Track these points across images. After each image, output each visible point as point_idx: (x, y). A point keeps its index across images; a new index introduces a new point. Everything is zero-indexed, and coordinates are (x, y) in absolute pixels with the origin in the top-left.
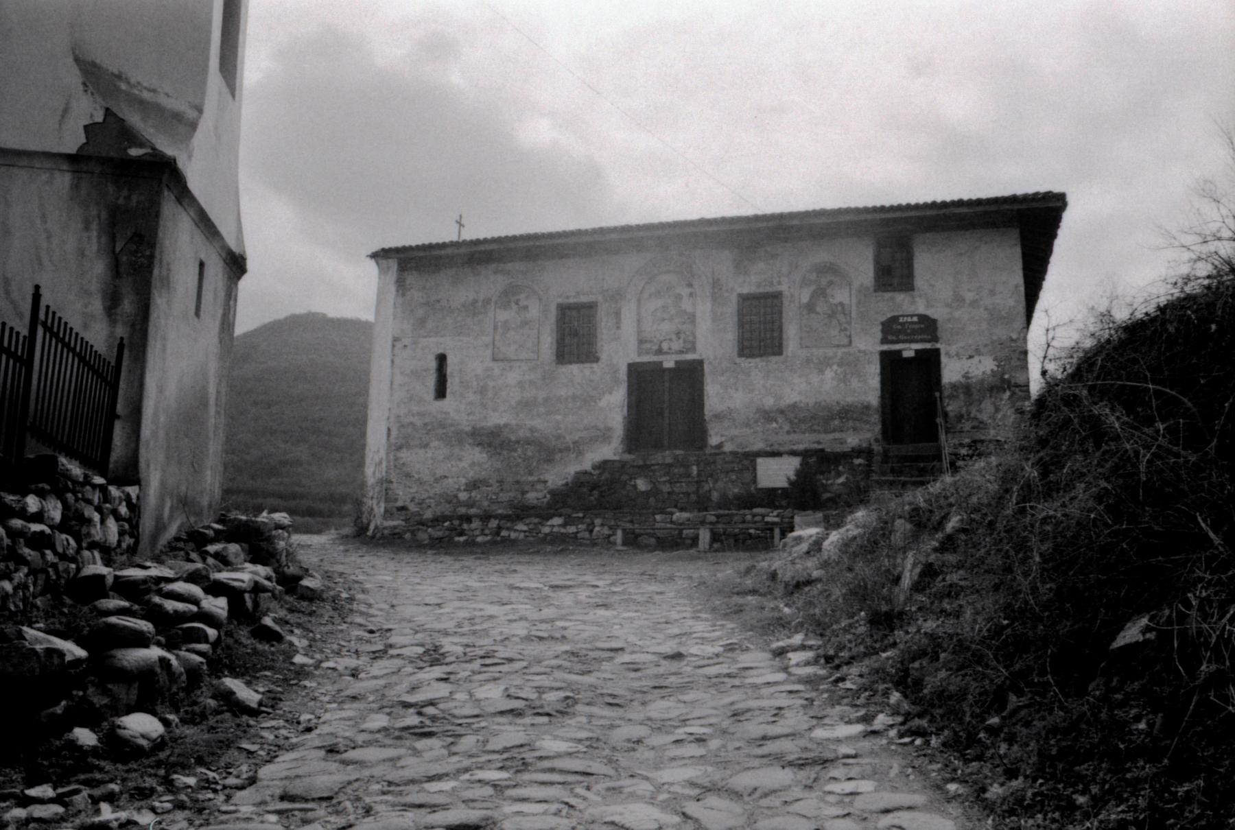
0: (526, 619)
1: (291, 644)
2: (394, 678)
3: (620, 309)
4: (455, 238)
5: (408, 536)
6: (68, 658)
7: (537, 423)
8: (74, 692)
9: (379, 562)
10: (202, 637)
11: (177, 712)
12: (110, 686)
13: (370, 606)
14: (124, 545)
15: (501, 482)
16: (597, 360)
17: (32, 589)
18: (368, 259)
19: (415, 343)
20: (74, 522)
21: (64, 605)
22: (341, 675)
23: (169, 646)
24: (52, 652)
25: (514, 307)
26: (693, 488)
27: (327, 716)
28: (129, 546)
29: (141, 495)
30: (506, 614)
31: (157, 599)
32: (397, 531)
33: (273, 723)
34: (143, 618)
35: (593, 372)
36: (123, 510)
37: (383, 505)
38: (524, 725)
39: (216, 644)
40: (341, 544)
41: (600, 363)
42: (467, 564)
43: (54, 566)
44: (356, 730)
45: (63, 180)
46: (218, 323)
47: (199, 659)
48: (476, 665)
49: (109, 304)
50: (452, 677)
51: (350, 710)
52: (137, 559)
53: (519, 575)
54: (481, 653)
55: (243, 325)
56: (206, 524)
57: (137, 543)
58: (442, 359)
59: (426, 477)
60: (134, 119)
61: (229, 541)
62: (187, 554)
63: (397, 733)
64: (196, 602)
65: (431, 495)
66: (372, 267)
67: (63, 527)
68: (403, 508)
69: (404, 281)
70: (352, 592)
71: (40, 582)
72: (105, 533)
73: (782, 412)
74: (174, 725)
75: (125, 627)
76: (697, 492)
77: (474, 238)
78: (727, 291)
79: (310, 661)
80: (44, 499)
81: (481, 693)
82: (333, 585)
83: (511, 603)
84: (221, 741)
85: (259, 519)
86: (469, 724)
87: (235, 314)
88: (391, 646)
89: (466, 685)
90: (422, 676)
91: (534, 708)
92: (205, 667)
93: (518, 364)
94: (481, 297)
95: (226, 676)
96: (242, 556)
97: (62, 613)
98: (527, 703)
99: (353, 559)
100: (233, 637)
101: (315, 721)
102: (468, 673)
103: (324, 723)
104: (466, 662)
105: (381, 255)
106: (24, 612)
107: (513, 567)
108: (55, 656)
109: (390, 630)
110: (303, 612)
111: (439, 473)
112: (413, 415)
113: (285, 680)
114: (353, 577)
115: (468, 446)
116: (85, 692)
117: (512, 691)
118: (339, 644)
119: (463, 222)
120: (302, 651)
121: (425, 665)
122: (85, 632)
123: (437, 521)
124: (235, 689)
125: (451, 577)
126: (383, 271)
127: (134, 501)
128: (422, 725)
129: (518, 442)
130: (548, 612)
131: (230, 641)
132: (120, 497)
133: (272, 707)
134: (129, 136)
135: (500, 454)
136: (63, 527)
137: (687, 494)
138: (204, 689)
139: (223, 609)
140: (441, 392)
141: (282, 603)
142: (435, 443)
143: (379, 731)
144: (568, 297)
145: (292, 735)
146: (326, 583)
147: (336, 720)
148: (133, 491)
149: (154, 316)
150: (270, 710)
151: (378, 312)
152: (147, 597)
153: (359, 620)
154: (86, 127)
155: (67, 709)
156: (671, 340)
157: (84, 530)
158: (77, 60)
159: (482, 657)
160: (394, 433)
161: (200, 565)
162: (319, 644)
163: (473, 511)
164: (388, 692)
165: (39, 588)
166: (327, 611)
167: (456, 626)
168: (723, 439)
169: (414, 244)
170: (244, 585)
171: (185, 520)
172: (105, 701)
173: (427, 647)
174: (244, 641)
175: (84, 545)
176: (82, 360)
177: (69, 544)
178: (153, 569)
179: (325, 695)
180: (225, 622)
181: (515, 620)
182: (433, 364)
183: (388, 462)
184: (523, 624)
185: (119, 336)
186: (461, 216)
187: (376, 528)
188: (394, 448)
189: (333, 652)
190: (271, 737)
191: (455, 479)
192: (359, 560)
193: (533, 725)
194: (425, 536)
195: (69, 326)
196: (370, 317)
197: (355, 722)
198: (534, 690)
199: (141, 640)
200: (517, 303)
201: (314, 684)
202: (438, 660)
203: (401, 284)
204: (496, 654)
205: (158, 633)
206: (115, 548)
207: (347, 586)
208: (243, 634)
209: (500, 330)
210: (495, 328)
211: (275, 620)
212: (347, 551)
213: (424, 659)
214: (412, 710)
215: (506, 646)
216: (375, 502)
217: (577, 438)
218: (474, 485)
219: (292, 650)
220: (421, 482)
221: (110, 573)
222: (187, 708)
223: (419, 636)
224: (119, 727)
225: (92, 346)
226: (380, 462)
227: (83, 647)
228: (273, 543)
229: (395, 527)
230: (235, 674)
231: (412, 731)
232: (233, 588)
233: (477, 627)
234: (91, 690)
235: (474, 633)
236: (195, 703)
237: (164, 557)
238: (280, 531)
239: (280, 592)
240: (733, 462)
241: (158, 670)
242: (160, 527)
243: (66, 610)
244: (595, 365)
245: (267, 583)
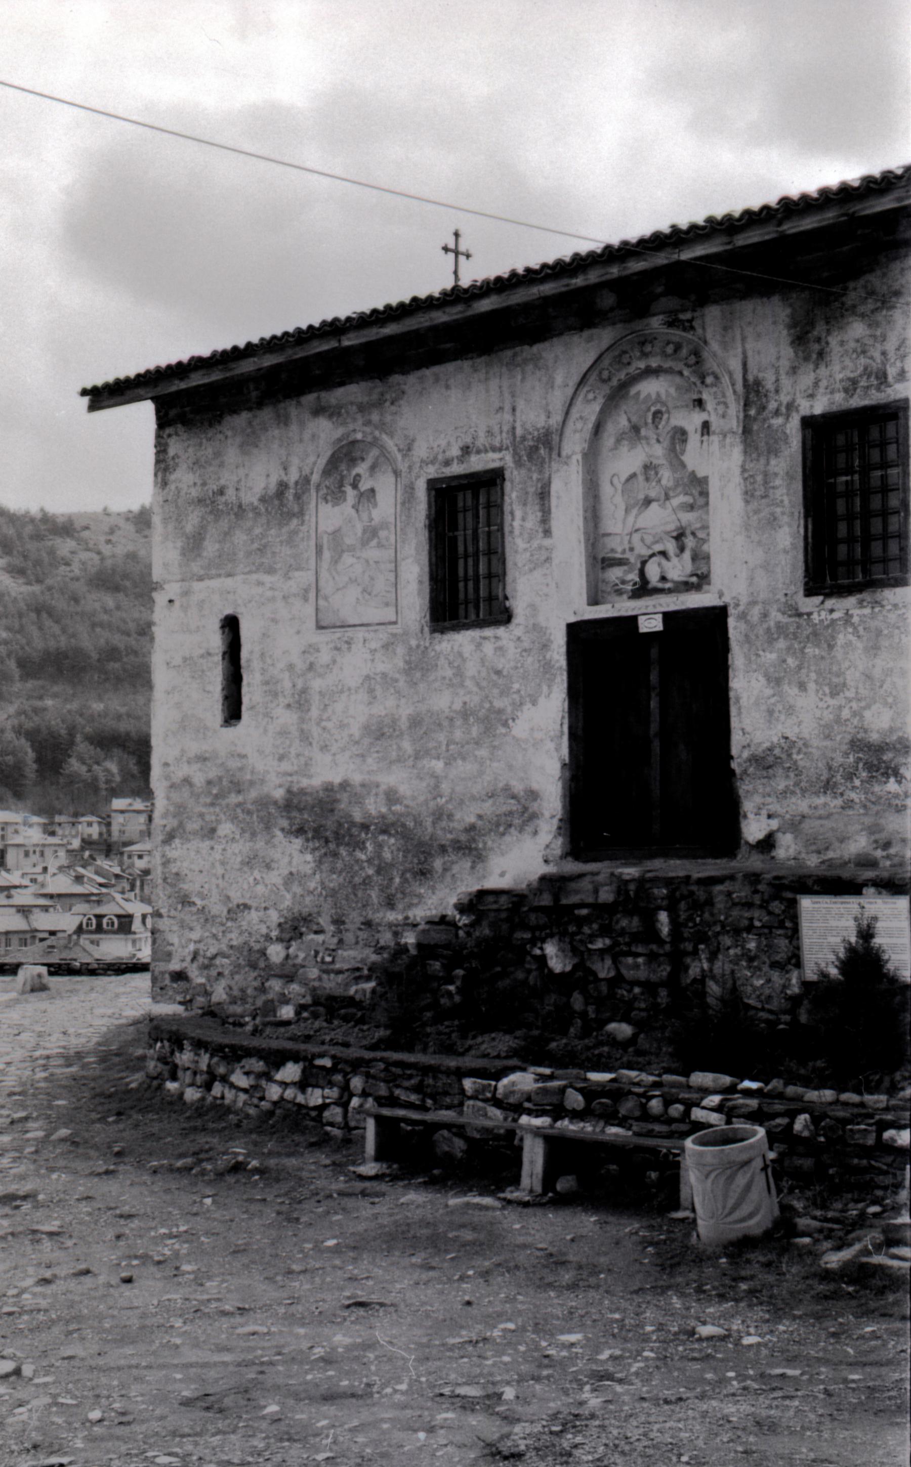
16: (504, 617)
19: (186, 593)
26: (664, 970)
41: (512, 626)
58: (231, 625)
59: (218, 909)
65: (224, 948)
68: (180, 976)
76: (673, 982)
78: (777, 413)
94: (293, 476)
111: (237, 897)
129: (365, 827)
135: (335, 855)
137: (650, 987)
144: (447, 463)
156: (663, 554)
168: (774, 824)
182: (216, 641)
200: (355, 486)
209: (327, 555)
217: (472, 819)
240: (749, 905)
244: (501, 631)
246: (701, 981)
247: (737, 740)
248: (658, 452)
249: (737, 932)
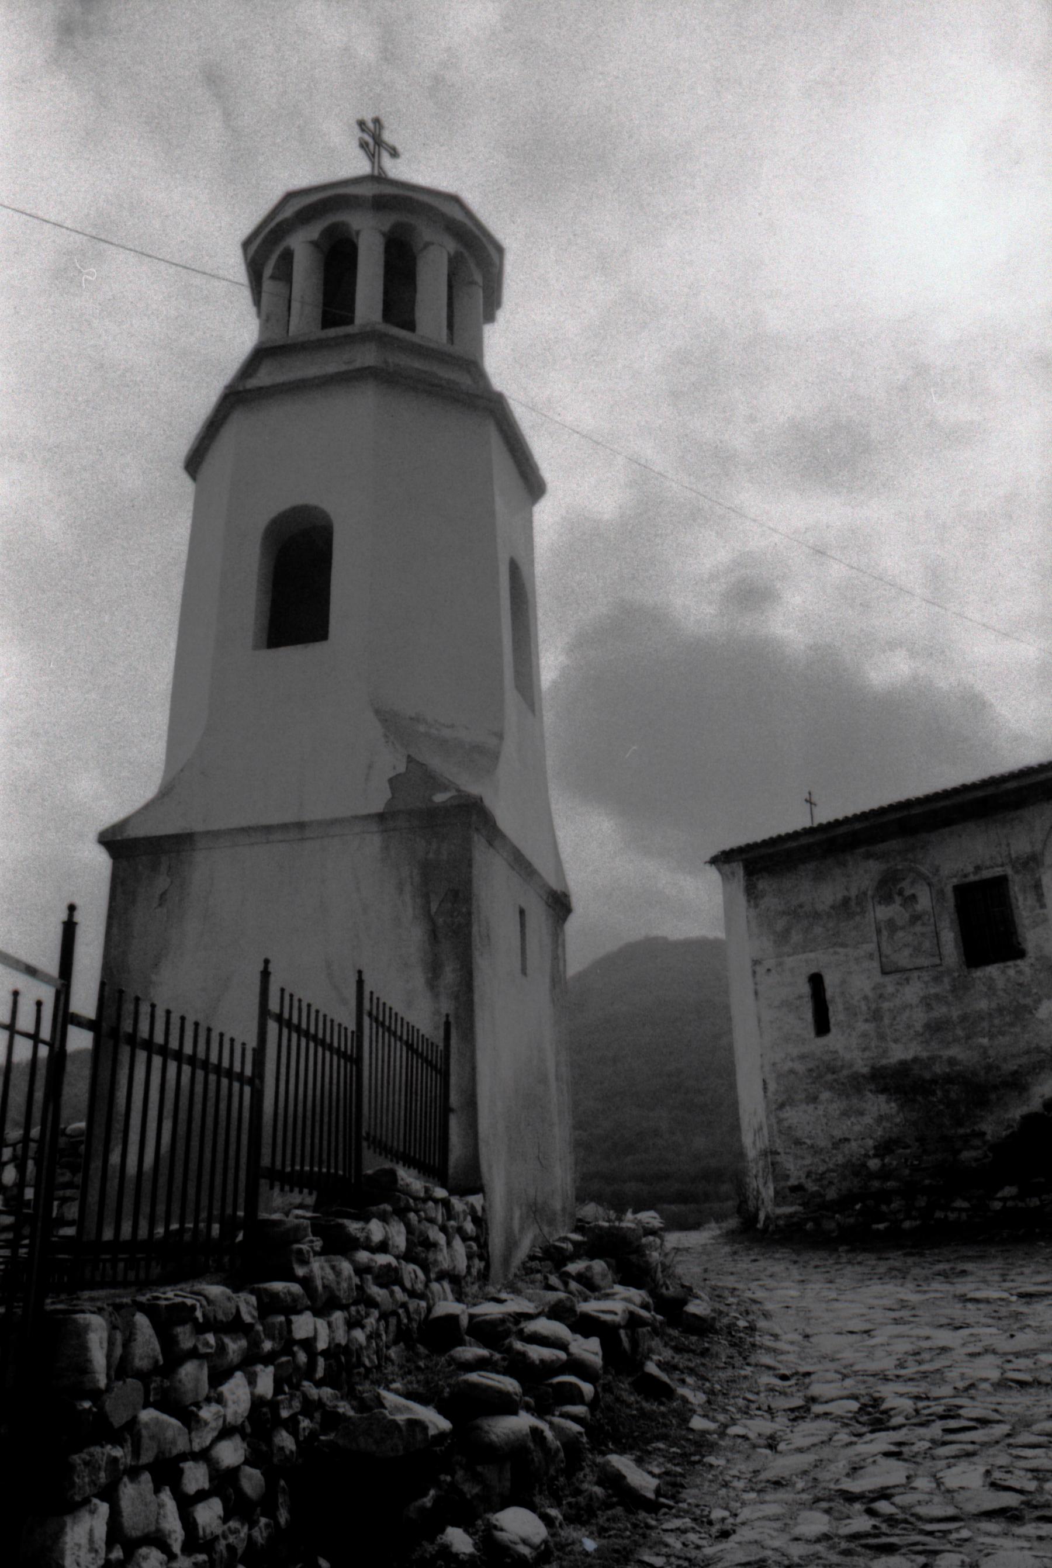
0: (994, 1352)
1: (685, 1400)
2: (826, 1452)
3: (1040, 880)
4: (808, 824)
5: (809, 1226)
6: (432, 1432)
7: (954, 1052)
8: (442, 1477)
9: (778, 1268)
10: (574, 1396)
11: (559, 1505)
12: (479, 1469)
13: (776, 1337)
14: (474, 1271)
15: (921, 1140)
16: (1021, 954)
17: (384, 1337)
18: (708, 867)
20: (420, 1249)
21: (418, 1355)
22: (754, 1446)
23: (541, 1410)
24: (415, 1424)
25: (898, 900)
27: (745, 1514)
28: (479, 1271)
29: (487, 1205)
30: (964, 1345)
31: (519, 1345)
32: (795, 1220)
33: (677, 1523)
34: (505, 1372)
35: (1020, 972)
36: (469, 1227)
37: (771, 1186)
38: (1028, 1538)
39: (593, 1404)
40: (726, 1244)
42: (897, 1264)
43: (404, 1305)
44: (787, 1537)
45: (374, 842)
46: (547, 980)
47: (576, 1428)
48: (936, 1429)
49: (430, 975)
50: (905, 1449)
51: (774, 1504)
52: (491, 1290)
53: (970, 1278)
54: (940, 1409)
55: (574, 965)
56: (562, 1235)
57: (488, 1267)
58: (816, 981)
59: (823, 1143)
60: (436, 763)
61: (592, 1258)
62: (546, 1278)
63: (844, 1545)
64: (563, 1346)
65: (831, 1166)
66: (713, 874)
67: (408, 1256)
69: (755, 887)
70: (751, 1317)
71: (392, 1328)
72: (453, 1259)
74: (557, 1524)
75: (489, 1388)
77: (831, 819)
79: (712, 1426)
80: (387, 1223)
81: (953, 1478)
82: (724, 1309)
83: (968, 1326)
84: (616, 1551)
85: (624, 1225)
86: (946, 1533)
87: (565, 966)
88: (813, 1400)
89: (928, 1463)
90: (861, 1448)
91: (1036, 1507)
92: (584, 1439)
93: (916, 974)
94: (853, 892)
95: (612, 1452)
96: (610, 1277)
97: (418, 1368)
98: (1023, 1498)
99: (745, 1266)
100: (612, 1393)
101: (731, 1520)
102: (928, 1445)
103: (743, 1524)
104: (921, 1425)
105: (722, 859)
106: (379, 1367)
107: (960, 1266)
108: (417, 1430)
109: (808, 1374)
110: (693, 1352)
111: (838, 1134)
112: (792, 1060)
113: (685, 1455)
114: (749, 1294)
115: (870, 1095)
116: (453, 1477)
117: (997, 1475)
118: (745, 1399)
119: (814, 799)
120: (699, 1410)
121: (864, 1429)
122: (446, 1395)
123: (844, 1202)
124: (625, 1471)
125: (876, 1288)
126: (726, 878)
127: (480, 1214)
128: (876, 1532)
129: (934, 1081)
130: (1025, 1340)
131: (609, 1398)
132: (464, 1211)
133: (673, 1497)
134: (432, 781)
136: (408, 1256)
138: (587, 1470)
139: (596, 1354)
140: (822, 1026)
141: (666, 1339)
142: (825, 1095)
143: (817, 1540)
144: (966, 876)
145: (704, 1543)
146: (717, 1306)
147: (759, 1519)
148: (476, 1200)
149: (477, 982)
150: (671, 1503)
151: (728, 929)
152: (507, 1341)
153: (767, 1360)
154: (390, 781)
155: (436, 1500)
157: (431, 1256)
158: (377, 712)
159: (942, 1418)
160: (772, 1086)
161: (562, 1295)
162: (720, 1398)
163: (891, 1184)
164: (824, 1475)
165: (391, 1336)
166: (722, 1348)
167: (896, 1366)
169: (759, 840)
170: (617, 1319)
171: (538, 1231)
172: (476, 1490)
173: (863, 1400)
174: (625, 1395)
175: (433, 1276)
176: (410, 1047)
177: (416, 1277)
178: (509, 1303)
179: (739, 1478)
180: (601, 1372)
181: (979, 1354)
182: (806, 989)
183: (770, 1126)
184: (990, 1359)
185: (444, 1012)
186: (810, 793)
187: (767, 1218)
188: (774, 1107)
189: (740, 1410)
190: (678, 1545)
191: (860, 1142)
192: (753, 1267)
193: (1040, 1538)
194: (832, 1225)
195: (393, 1012)
196: (720, 934)
197: (785, 1522)
198: (1029, 1475)
199: (507, 1405)
201: (722, 1462)
202: (879, 1421)
203: (751, 892)
204: (962, 1412)
205: (525, 1392)
206: (465, 1277)
207: (743, 1309)
208: (624, 1387)
209: (885, 933)
210: (879, 932)
211: (659, 1365)
212: (735, 1253)
213: (862, 1419)
214: (858, 1506)
215: (972, 1398)
216: (761, 1181)
218: (885, 1148)
219: (685, 1413)
220: (815, 1150)
221: (463, 1312)
222: (570, 1499)
223: (848, 1382)
224: (495, 1527)
225: (418, 1030)
226: (761, 1129)
227: (446, 1417)
228: (644, 1255)
229: (791, 1215)
230: (622, 1451)
231: (864, 1542)
232: (605, 1322)
233: (924, 1367)
234: (460, 1474)
235: (925, 1375)
236: (578, 1492)
237: (520, 1285)
238: (651, 1238)
239: (661, 1323)
241: (531, 1445)
242: (511, 1245)
243: (421, 1364)
244: (1019, 962)
245: (644, 1313)
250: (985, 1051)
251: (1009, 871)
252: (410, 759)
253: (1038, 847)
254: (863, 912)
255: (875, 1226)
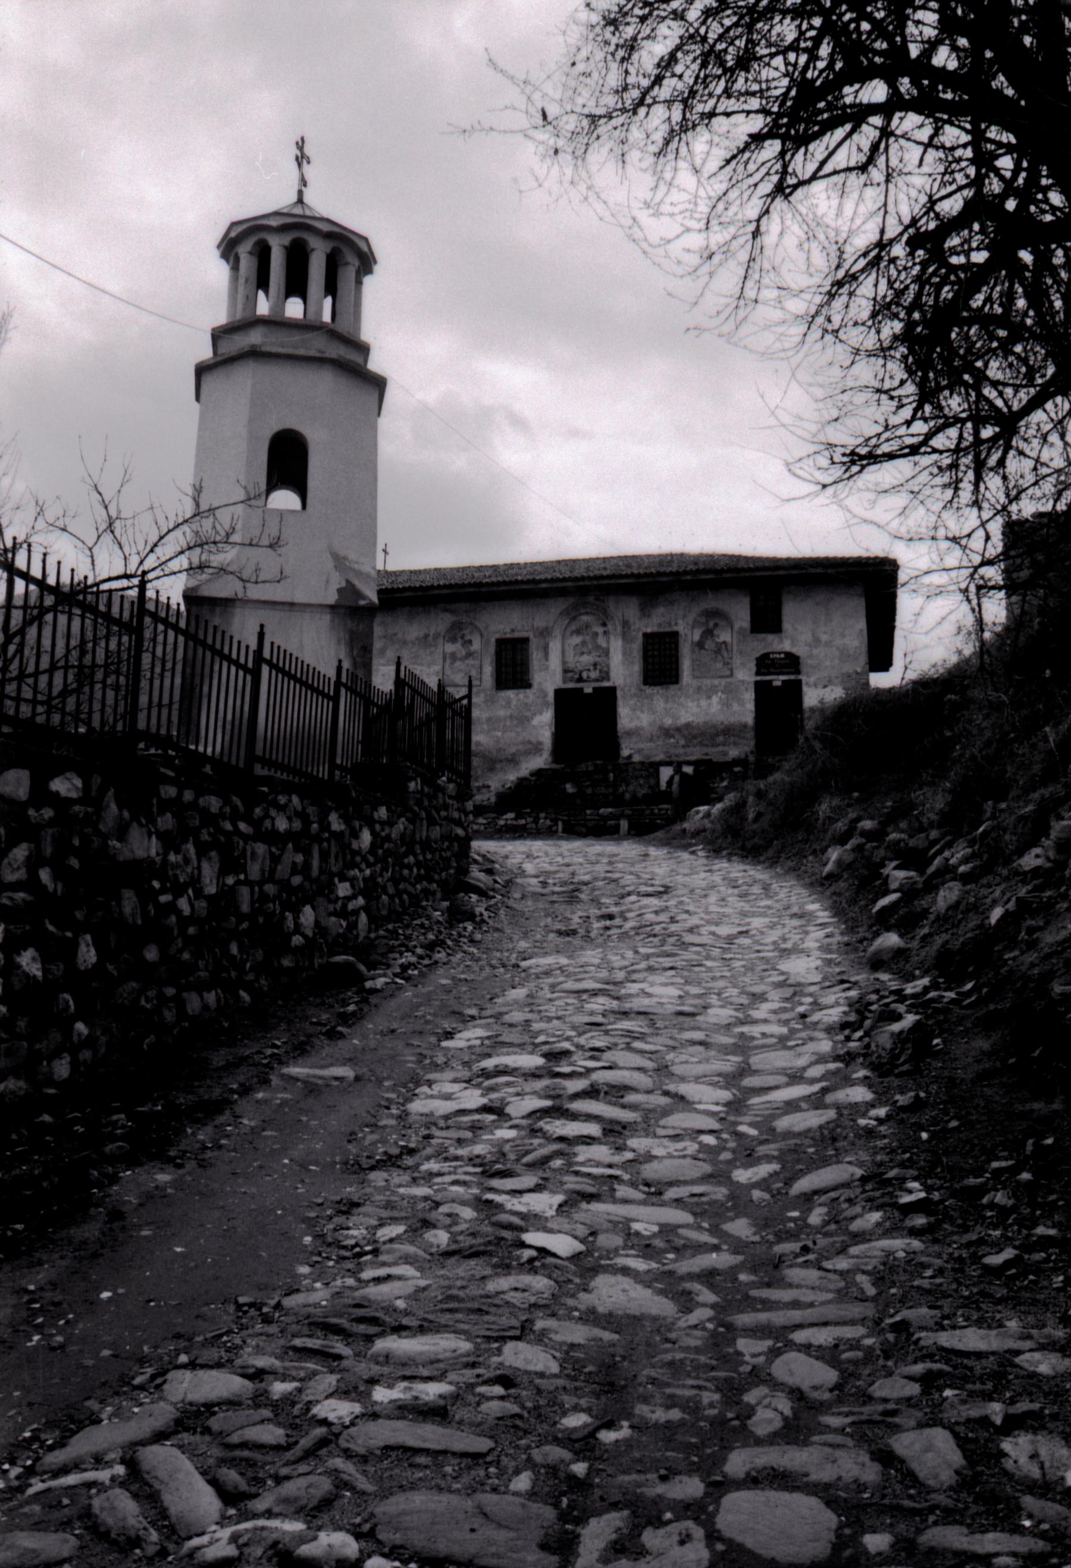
16: (529, 686)
25: (460, 641)
45: (327, 618)
73: (678, 729)
209: (448, 661)
246: (623, 793)
247: (619, 726)
248: (588, 638)
249: (637, 778)
250: (498, 741)
251: (531, 635)
252: (348, 581)
253: (551, 624)
254: (436, 646)
255: (115, 973)
